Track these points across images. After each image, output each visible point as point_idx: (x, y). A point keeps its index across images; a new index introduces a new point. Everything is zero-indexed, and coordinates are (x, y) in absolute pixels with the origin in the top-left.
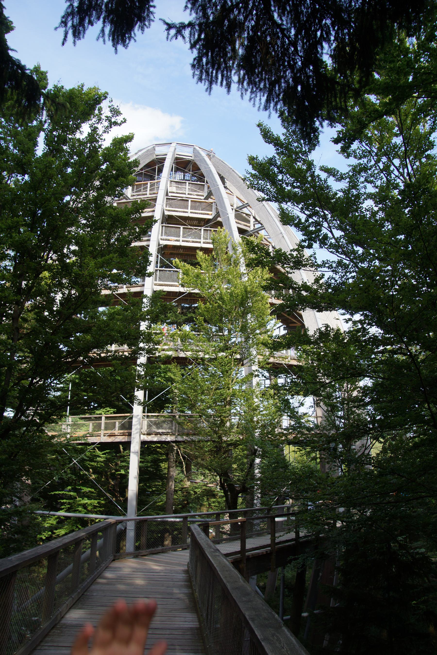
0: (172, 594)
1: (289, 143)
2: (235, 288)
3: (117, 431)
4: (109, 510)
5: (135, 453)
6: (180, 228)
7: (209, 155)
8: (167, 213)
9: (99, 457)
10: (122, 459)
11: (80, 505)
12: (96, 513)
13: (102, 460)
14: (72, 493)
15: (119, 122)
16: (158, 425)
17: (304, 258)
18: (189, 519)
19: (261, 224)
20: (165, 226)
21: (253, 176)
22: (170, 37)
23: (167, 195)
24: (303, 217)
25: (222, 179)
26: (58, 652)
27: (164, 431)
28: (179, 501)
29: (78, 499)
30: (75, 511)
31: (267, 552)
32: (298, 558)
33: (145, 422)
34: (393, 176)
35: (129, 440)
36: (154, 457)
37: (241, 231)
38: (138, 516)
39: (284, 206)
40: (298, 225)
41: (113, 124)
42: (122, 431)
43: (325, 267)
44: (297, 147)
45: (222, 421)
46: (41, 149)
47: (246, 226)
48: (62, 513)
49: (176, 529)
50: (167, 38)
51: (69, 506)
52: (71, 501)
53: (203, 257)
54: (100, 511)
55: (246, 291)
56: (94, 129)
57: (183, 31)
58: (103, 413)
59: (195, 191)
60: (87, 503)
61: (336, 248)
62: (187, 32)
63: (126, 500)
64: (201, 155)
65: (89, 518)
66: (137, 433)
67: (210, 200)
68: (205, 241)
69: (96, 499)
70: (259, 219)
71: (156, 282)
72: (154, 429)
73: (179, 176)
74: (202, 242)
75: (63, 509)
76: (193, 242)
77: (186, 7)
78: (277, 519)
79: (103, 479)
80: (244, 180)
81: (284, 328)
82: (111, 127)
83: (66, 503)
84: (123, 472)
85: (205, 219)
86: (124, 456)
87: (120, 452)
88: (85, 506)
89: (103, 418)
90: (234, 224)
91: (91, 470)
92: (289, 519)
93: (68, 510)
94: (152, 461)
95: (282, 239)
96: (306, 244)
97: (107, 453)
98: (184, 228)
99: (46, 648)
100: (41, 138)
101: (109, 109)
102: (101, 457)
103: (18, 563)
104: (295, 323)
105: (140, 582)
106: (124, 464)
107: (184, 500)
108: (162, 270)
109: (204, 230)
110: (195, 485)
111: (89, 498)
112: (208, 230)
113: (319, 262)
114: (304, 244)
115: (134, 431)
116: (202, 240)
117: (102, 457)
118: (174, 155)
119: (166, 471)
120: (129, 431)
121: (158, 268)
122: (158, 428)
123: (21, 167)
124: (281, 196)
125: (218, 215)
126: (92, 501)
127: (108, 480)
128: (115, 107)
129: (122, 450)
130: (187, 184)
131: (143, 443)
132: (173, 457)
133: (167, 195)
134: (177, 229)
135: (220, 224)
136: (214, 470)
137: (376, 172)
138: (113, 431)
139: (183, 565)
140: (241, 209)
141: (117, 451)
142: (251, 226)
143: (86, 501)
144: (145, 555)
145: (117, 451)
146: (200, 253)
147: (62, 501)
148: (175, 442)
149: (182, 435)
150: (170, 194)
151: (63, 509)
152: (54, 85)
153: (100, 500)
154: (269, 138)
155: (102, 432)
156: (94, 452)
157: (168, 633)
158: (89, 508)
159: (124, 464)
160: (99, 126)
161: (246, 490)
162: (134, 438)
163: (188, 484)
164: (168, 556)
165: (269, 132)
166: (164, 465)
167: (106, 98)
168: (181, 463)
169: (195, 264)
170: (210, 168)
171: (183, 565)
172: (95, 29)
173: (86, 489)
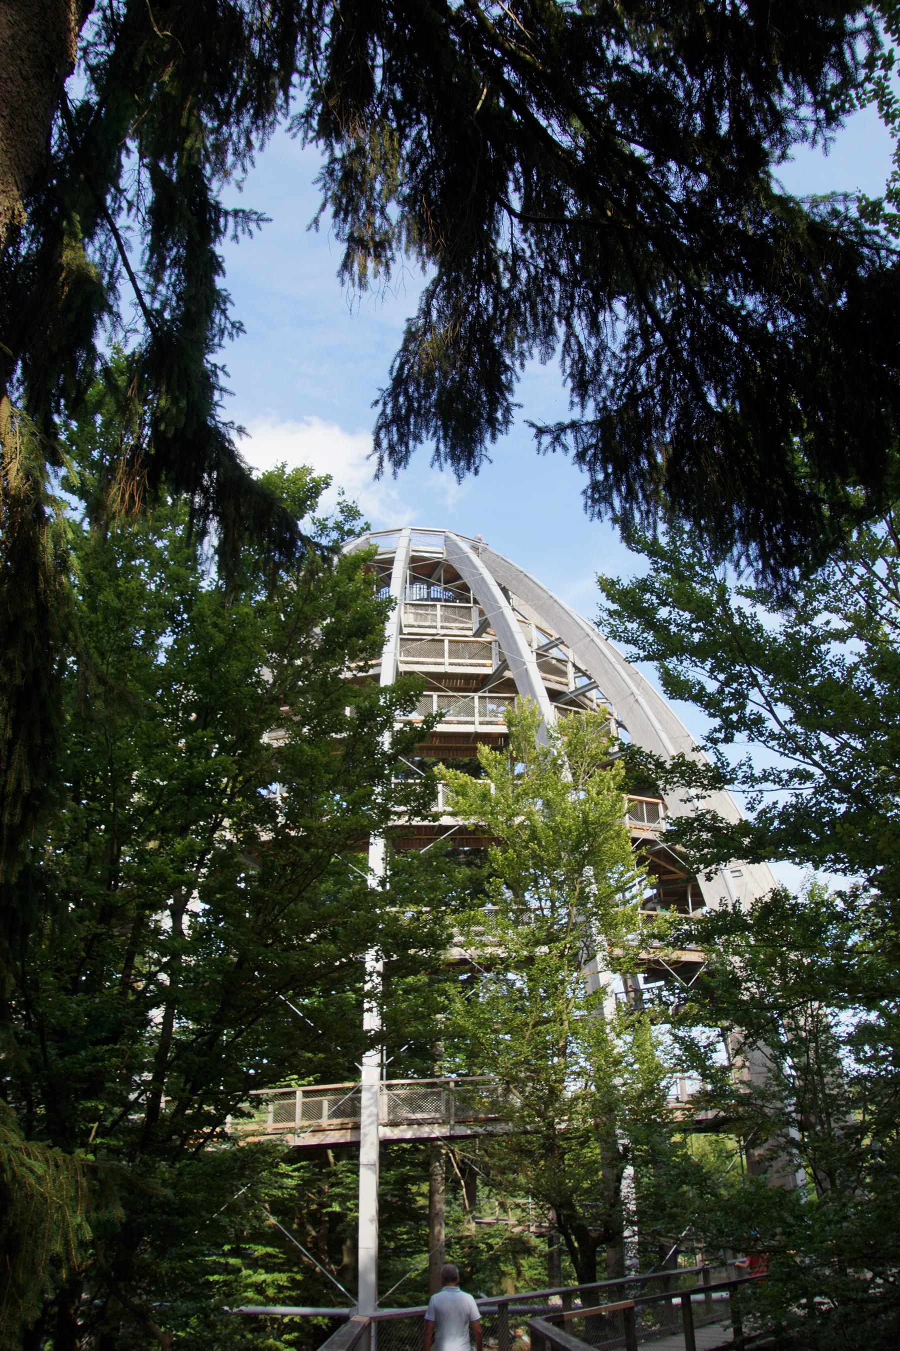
2: (563, 816)
4: (309, 1291)
7: (475, 549)
8: (403, 668)
10: (333, 1180)
11: (248, 1286)
12: (284, 1303)
14: (232, 1261)
15: (357, 530)
16: (412, 1103)
18: (511, 1307)
19: (590, 678)
21: (611, 613)
22: (543, 447)
23: (401, 633)
24: (712, 686)
25: (505, 591)
29: (245, 1272)
33: (384, 1099)
34: (879, 598)
37: (554, 695)
38: (382, 1305)
39: (672, 663)
40: (699, 697)
43: (767, 780)
45: (552, 1091)
50: (538, 450)
52: (232, 1277)
53: (491, 757)
54: (290, 1298)
55: (585, 821)
57: (563, 437)
59: (455, 621)
61: (788, 743)
62: (569, 438)
67: (486, 638)
69: (284, 1272)
70: (583, 668)
73: (419, 591)
76: (459, 723)
77: (572, 403)
80: (599, 624)
84: (336, 1208)
86: (335, 1174)
87: (328, 1164)
88: (259, 1288)
89: (299, 1094)
90: (539, 683)
92: (708, 1297)
94: (396, 1182)
95: (635, 705)
96: (721, 736)
102: (291, 1177)
110: (487, 1230)
113: (757, 773)
114: (718, 735)
116: (477, 719)
117: (291, 1178)
119: (422, 1201)
126: (276, 1275)
129: (332, 1159)
131: (385, 1144)
132: (438, 1168)
133: (401, 633)
135: (510, 686)
137: (844, 592)
141: (329, 1163)
142: (572, 683)
143: (262, 1276)
145: (329, 1163)
146: (484, 750)
147: (211, 1278)
148: (451, 1139)
150: (406, 630)
153: (291, 1271)
154: (638, 543)
158: (271, 1292)
161: (613, 1236)
163: (470, 1228)
167: (328, 484)
169: (476, 770)
170: (482, 573)
172: (425, 449)
173: (260, 1250)
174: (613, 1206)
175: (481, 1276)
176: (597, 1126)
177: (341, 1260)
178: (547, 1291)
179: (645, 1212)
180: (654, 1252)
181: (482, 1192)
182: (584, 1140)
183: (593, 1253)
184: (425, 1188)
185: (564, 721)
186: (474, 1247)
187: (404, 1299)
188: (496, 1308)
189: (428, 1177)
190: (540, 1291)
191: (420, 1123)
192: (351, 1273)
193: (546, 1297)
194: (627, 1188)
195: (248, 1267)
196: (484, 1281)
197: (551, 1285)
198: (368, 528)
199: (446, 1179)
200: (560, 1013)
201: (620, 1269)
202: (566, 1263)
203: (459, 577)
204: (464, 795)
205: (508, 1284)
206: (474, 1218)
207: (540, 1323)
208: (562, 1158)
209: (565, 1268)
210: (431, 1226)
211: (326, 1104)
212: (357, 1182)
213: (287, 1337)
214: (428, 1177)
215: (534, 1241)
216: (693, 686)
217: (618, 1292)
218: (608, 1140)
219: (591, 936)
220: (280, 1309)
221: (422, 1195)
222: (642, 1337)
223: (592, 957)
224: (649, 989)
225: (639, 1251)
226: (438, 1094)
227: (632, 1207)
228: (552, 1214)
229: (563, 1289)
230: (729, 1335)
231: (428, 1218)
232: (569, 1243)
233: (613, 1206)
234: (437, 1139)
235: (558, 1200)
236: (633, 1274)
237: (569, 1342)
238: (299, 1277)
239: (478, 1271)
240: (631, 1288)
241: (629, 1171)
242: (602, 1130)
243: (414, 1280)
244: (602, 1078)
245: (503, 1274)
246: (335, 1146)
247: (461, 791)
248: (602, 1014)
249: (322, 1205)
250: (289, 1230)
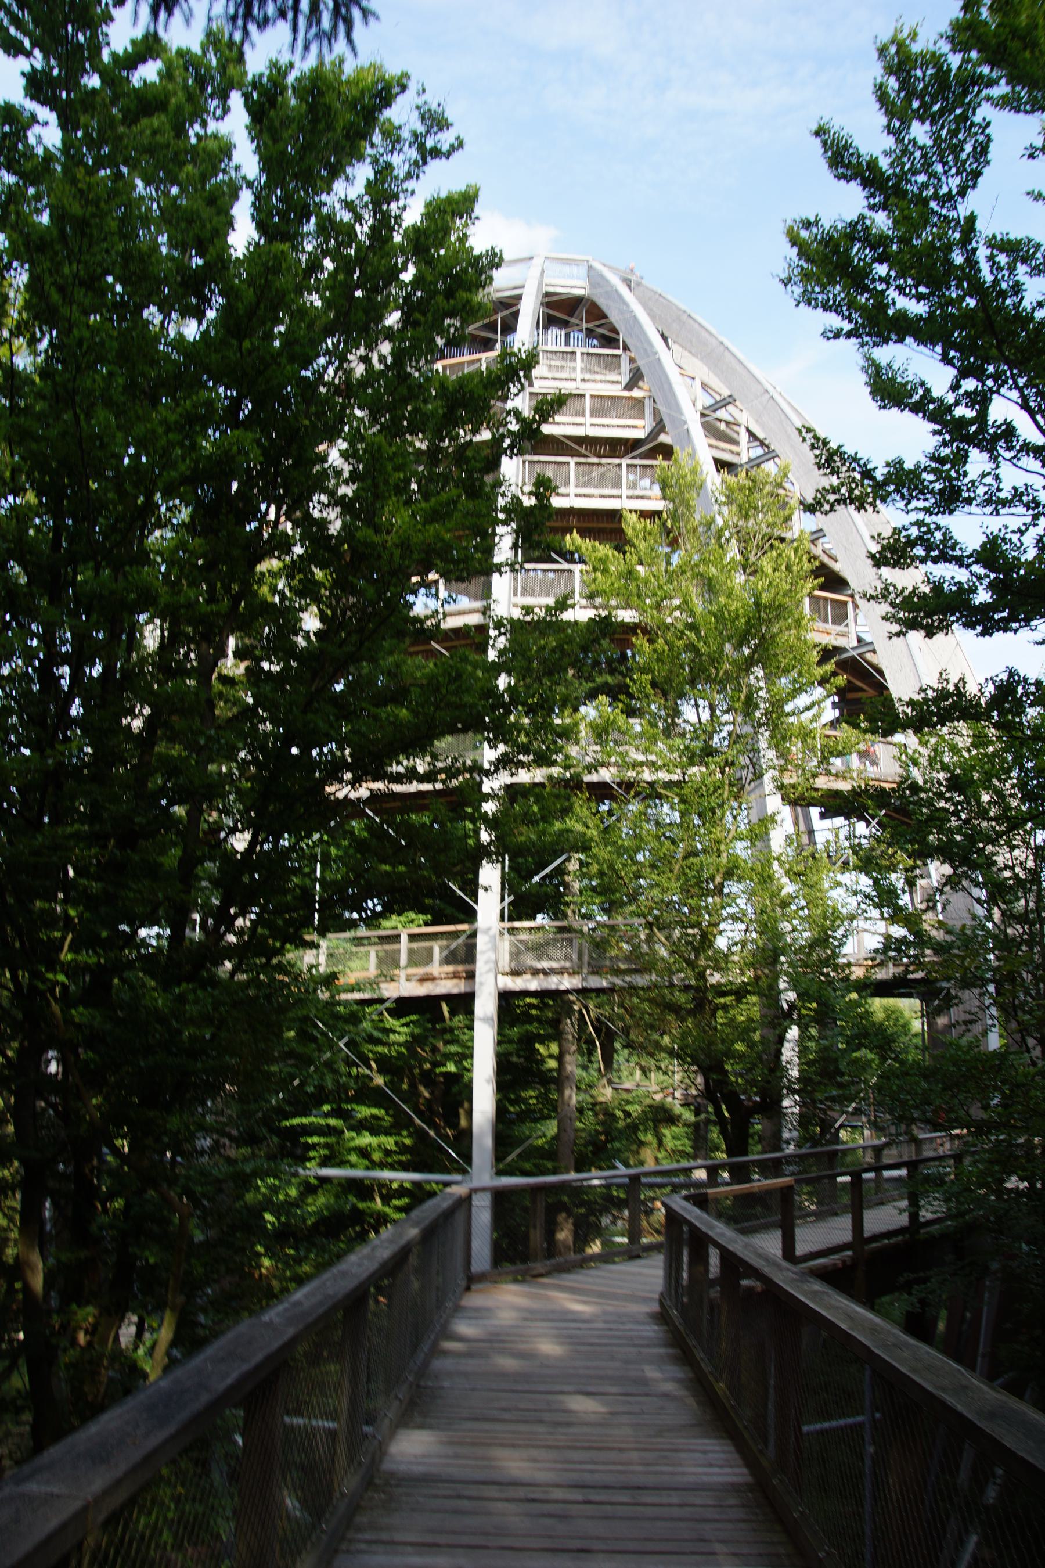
0: (643, 1381)
1: (902, 177)
2: (729, 596)
3: (435, 968)
4: (422, 1156)
5: (485, 1020)
7: (628, 283)
9: (394, 1032)
10: (448, 1037)
11: (350, 1150)
12: (392, 1167)
13: (401, 1039)
14: (332, 1122)
15: (445, 148)
16: (539, 949)
17: (966, 481)
20: (530, 462)
25: (664, 337)
26: (397, 1560)
27: (554, 965)
28: (590, 1135)
29: (348, 1134)
30: (342, 1164)
31: (844, 1262)
32: (925, 1281)
33: (505, 945)
35: (468, 990)
36: (527, 1031)
38: (500, 1173)
40: (925, 406)
41: (428, 154)
44: (924, 186)
45: (704, 935)
46: (242, 236)
47: (732, 452)
48: (313, 1170)
49: (582, 1204)
52: (332, 1140)
53: (639, 527)
54: (400, 1163)
56: (384, 171)
58: (400, 926)
64: (607, 281)
65: (374, 1179)
67: (636, 393)
68: (630, 493)
69: (391, 1135)
72: (530, 961)
74: (624, 497)
78: (840, 1179)
81: (834, 703)
82: (425, 163)
83: (319, 1144)
84: (451, 1067)
85: (627, 440)
86: (451, 1030)
88: (364, 1153)
89: (404, 938)
90: (703, 451)
91: (373, 1064)
93: (325, 1163)
94: (520, 1040)
97: (412, 1022)
98: (577, 464)
99: (363, 1546)
100: (243, 210)
101: (416, 113)
102: (399, 1033)
103: (291, 1332)
104: (861, 690)
105: (549, 1348)
106: (453, 1049)
109: (628, 466)
110: (625, 1096)
111: (374, 1132)
112: (635, 466)
115: (482, 966)
116: (625, 492)
117: (400, 1031)
118: (540, 284)
119: (552, 1064)
120: (468, 967)
122: (539, 958)
123: (188, 295)
124: (879, 325)
125: (660, 427)
126: (383, 1139)
127: (416, 1088)
128: (434, 107)
131: (505, 998)
132: (569, 1027)
134: (563, 468)
135: (667, 451)
136: (691, 1056)
138: (427, 969)
139: (645, 1300)
140: (714, 411)
141: (439, 1017)
142: (745, 452)
143: (366, 1139)
144: (541, 1275)
145: (439, 1017)
147: (310, 1140)
148: (583, 992)
149: (596, 971)
152: (271, 61)
153: (400, 1134)
154: (847, 166)
156: (382, 1021)
157: (675, 1500)
158: (376, 1156)
159: (453, 1049)
160: (396, 160)
161: (771, 1108)
162: (481, 984)
163: (606, 1094)
164: (598, 1277)
165: (846, 148)
167: (404, 88)
168: (590, 1042)
170: (632, 312)
171: (645, 1300)
173: (364, 1111)
174: (772, 1071)
175: (617, 1145)
176: (757, 978)
177: (459, 1123)
178: (692, 1163)
179: (810, 1079)
180: (817, 1125)
181: (621, 1056)
182: (740, 993)
183: (747, 1124)
184: (554, 1048)
185: (731, 479)
186: (610, 1116)
187: (527, 1166)
188: (627, 1180)
189: (557, 1036)
190: (685, 1164)
191: (545, 973)
192: (464, 1138)
193: (688, 1171)
194: (789, 1053)
195: (351, 1128)
196: (619, 1151)
197: (695, 1157)
198: (461, 145)
199: (579, 1039)
200: (718, 842)
201: (776, 1142)
202: (714, 1134)
203: (605, 316)
204: (605, 571)
205: (648, 1155)
206: (610, 1082)
207: (679, 1203)
208: (713, 1015)
209: (712, 1141)
210: (561, 1092)
211: (436, 951)
212: (472, 1039)
213: (396, 1202)
214: (557, 1036)
215: (678, 1109)
216: (914, 391)
217: (772, 1168)
218: (771, 995)
219: (758, 751)
220: (386, 1174)
221: (551, 1056)
222: (800, 1218)
223: (758, 776)
224: (827, 830)
225: (800, 1123)
226: (570, 941)
227: (795, 1073)
228: (700, 1080)
229: (709, 1162)
230: (904, 1220)
231: (558, 1080)
232: (718, 1112)
233: (772, 1071)
234: (567, 992)
235: (707, 1060)
236: (791, 1149)
237: (712, 1228)
238: (408, 1141)
239: (612, 1140)
240: (788, 1163)
241: (793, 1032)
242: (764, 983)
243: (541, 1148)
244: (767, 928)
245: (642, 1144)
246: (448, 998)
247: (601, 566)
248: (769, 847)
249: (435, 1064)
250: (397, 1091)
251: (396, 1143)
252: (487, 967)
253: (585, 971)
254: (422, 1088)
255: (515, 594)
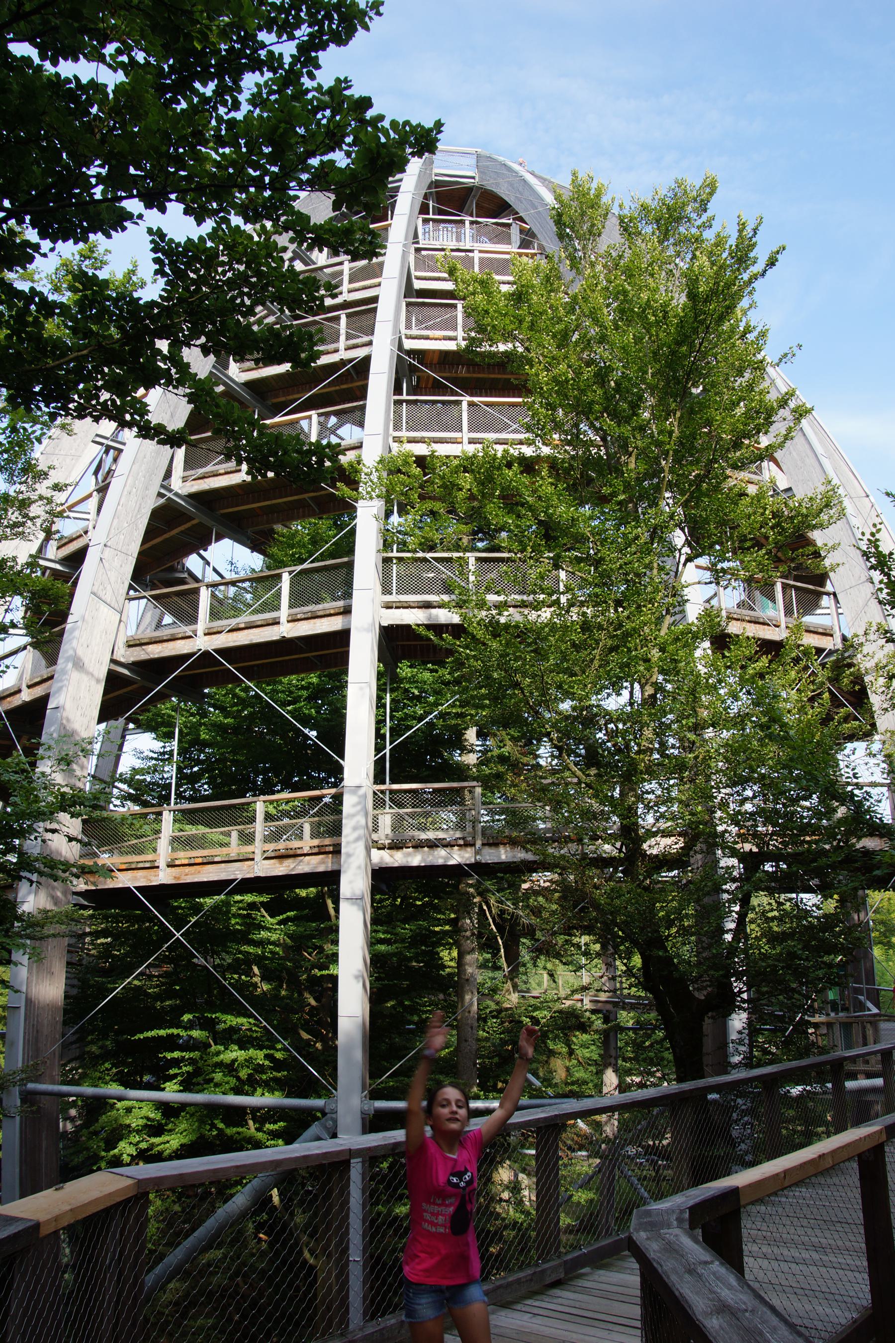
3: (308, 842)
6: (454, 306)
8: (408, 344)
11: (220, 1065)
14: (195, 1033)
28: (494, 1045)
35: (335, 868)
36: (420, 927)
38: (375, 1095)
42: (316, 842)
48: (171, 1093)
51: (189, 1068)
52: (195, 1055)
54: (275, 1079)
60: (234, 1061)
63: (332, 1051)
66: (357, 839)
71: (388, 598)
75: (175, 1076)
79: (283, 993)
88: (230, 1068)
107: (504, 1042)
108: (416, 401)
120: (334, 840)
121: (404, 397)
126: (252, 1052)
130: (467, 223)
131: (382, 878)
143: (234, 1054)
147: (169, 1056)
148: (478, 868)
151: (175, 1076)
155: (258, 847)
162: (349, 855)
166: (448, 956)
173: (231, 1020)
191: (432, 845)
210: (461, 997)
213: (269, 1126)
238: (279, 1055)
245: (552, 1053)
251: (267, 1057)
252: (355, 835)
253: (479, 843)
254: (306, 995)
255: (397, 427)
